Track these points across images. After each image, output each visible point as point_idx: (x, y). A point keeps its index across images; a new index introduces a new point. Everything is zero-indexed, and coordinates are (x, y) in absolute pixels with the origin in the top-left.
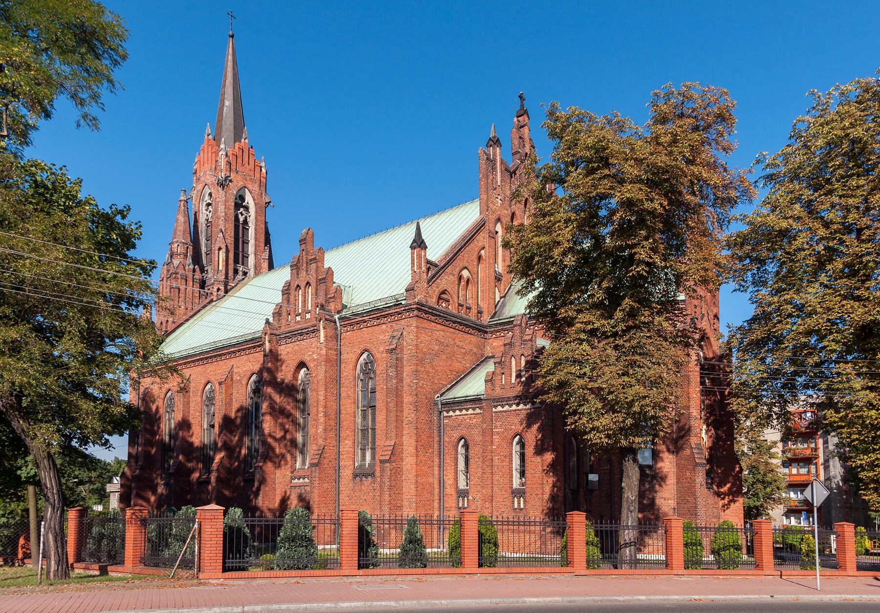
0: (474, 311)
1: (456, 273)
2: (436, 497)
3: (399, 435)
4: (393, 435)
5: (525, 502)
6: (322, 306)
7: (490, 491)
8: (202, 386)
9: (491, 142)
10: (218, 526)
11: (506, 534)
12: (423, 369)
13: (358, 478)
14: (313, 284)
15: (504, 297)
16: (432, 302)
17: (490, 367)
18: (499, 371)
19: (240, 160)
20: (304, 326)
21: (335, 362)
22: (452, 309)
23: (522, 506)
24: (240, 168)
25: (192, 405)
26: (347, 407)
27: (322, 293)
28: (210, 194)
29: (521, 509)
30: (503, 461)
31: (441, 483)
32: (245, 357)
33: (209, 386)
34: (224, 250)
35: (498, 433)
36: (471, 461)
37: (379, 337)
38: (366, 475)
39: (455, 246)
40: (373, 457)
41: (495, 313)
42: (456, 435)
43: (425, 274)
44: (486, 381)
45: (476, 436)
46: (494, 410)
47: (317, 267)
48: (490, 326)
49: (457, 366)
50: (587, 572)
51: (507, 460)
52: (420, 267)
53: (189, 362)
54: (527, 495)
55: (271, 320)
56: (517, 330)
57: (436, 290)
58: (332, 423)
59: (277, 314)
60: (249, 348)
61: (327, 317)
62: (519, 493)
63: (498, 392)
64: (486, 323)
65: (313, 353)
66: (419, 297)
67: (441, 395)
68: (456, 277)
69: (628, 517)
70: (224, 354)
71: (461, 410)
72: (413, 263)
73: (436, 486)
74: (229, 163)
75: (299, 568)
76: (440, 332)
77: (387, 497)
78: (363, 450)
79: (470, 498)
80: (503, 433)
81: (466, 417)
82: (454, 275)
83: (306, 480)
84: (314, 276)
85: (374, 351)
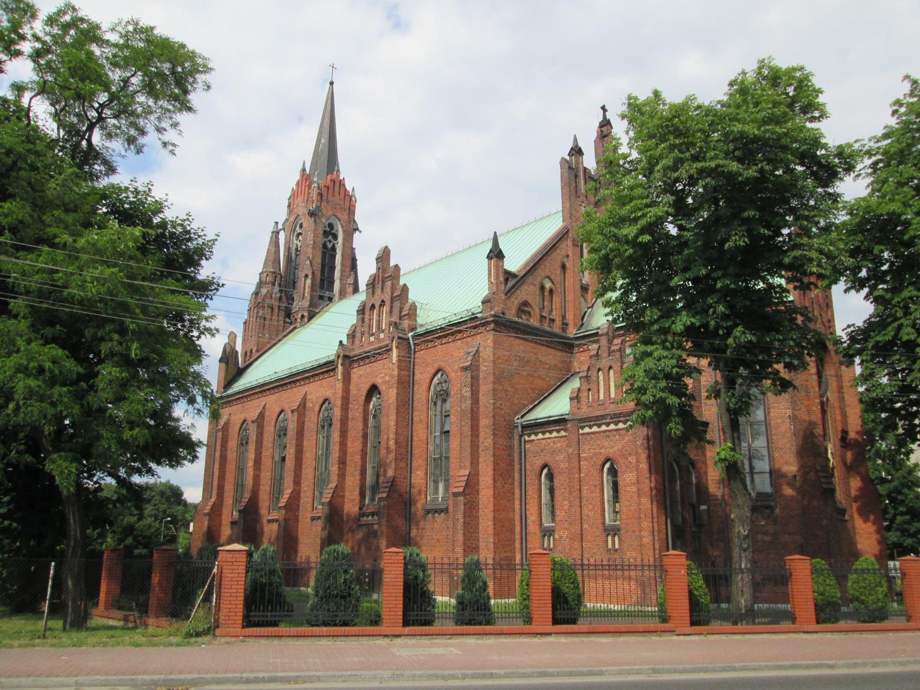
0: (558, 323)
1: (537, 283)
2: (517, 537)
3: (475, 463)
4: (468, 464)
5: (620, 540)
6: (396, 324)
7: (579, 528)
8: (276, 415)
9: (573, 152)
10: (240, 571)
11: (600, 581)
12: (501, 388)
13: (430, 515)
14: (388, 303)
15: (592, 307)
16: (511, 315)
17: (575, 384)
18: (584, 388)
19: (331, 191)
20: (377, 346)
21: (406, 383)
22: (534, 322)
23: (617, 546)
24: (330, 198)
25: (265, 436)
26: (420, 433)
27: (396, 311)
28: (301, 226)
29: (616, 550)
30: (592, 492)
31: (524, 519)
32: (319, 383)
33: (282, 415)
34: (310, 277)
35: (586, 459)
36: (557, 492)
37: (454, 355)
38: (439, 511)
39: (536, 255)
40: (446, 488)
41: (582, 324)
42: (539, 462)
43: (503, 286)
44: (571, 399)
45: (561, 463)
46: (581, 431)
47: (393, 284)
48: (577, 339)
49: (540, 383)
50: (550, 628)
51: (598, 490)
52: (497, 278)
53: (265, 391)
54: (623, 531)
55: (345, 342)
56: (604, 341)
57: (515, 302)
58: (403, 451)
59: (352, 336)
60: (323, 373)
61: (401, 335)
62: (613, 531)
63: (585, 411)
64: (572, 336)
65: (386, 375)
66: (496, 309)
67: (522, 417)
68: (538, 286)
69: (740, 557)
70: (298, 381)
71: (544, 433)
72: (490, 274)
73: (517, 523)
74: (321, 195)
75: (335, 625)
76: (518, 346)
77: (460, 537)
78: (436, 482)
79: (557, 536)
80: (592, 458)
81: (549, 441)
82: (535, 285)
83: (376, 517)
84: (389, 293)
85: (448, 369)
